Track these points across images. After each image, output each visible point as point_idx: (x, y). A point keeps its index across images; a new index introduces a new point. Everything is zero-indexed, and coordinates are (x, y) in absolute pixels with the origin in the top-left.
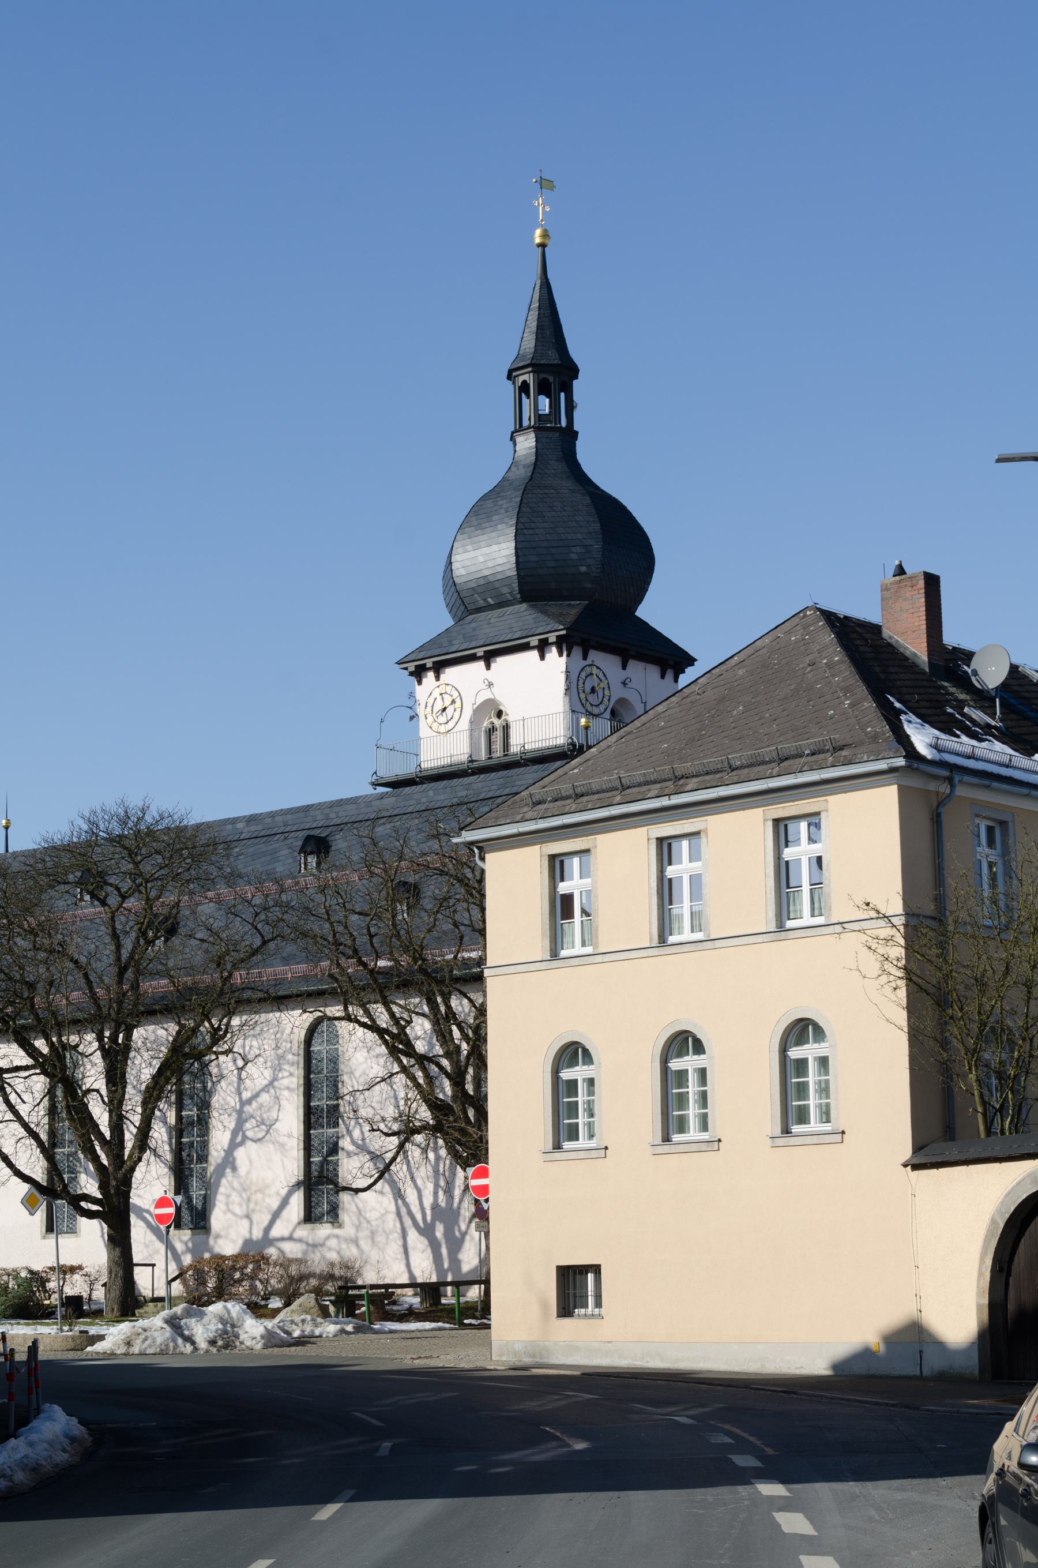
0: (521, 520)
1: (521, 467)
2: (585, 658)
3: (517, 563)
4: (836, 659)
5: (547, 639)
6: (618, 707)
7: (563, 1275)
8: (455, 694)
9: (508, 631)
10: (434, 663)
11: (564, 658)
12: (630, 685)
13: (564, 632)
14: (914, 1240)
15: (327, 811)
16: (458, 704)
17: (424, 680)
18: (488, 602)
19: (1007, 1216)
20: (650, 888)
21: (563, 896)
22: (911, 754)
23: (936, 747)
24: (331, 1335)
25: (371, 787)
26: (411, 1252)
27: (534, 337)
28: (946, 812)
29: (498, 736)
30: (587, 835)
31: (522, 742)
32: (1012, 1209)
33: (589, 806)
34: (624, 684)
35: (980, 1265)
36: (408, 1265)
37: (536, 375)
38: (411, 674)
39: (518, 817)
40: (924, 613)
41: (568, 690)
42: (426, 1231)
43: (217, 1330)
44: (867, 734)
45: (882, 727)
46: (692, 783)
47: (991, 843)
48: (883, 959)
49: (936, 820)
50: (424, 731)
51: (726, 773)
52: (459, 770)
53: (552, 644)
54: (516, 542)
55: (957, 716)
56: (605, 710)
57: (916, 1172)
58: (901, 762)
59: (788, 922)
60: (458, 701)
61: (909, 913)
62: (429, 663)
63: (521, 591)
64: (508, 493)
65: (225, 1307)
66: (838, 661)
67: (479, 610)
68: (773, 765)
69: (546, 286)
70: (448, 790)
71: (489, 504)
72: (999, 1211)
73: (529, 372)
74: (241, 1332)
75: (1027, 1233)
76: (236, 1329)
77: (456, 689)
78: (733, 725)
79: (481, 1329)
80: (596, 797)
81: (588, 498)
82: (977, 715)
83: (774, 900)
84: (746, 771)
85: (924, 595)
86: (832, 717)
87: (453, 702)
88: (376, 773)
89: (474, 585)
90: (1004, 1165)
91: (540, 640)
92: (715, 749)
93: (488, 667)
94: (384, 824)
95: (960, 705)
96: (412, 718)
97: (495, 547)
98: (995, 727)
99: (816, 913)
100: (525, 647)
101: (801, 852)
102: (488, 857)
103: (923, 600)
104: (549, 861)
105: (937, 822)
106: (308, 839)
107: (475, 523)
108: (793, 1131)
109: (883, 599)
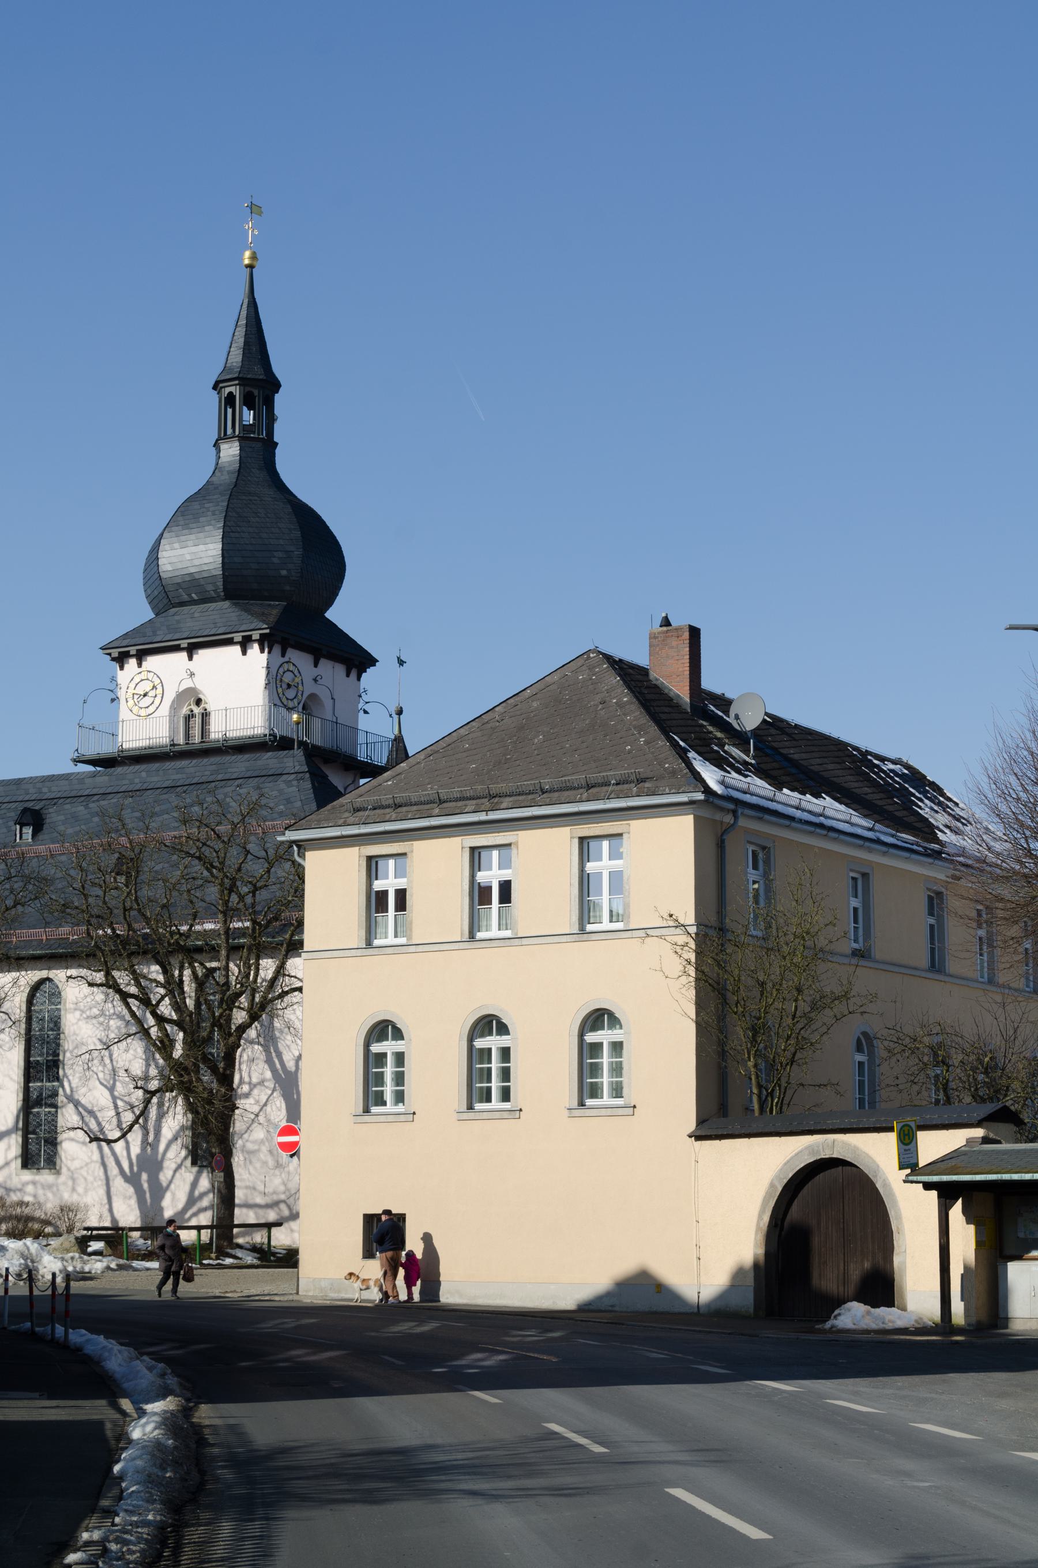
0: (227, 523)
1: (225, 473)
2: (283, 655)
3: (223, 563)
4: (625, 699)
5: (251, 636)
6: (308, 701)
7: (368, 1222)
8: (157, 681)
9: (212, 626)
10: (138, 650)
11: (266, 654)
12: (320, 682)
13: (268, 631)
14: (696, 1199)
15: (39, 785)
16: (159, 690)
17: (126, 666)
18: (192, 597)
19: (785, 1181)
20: (462, 891)
21: (377, 892)
22: (707, 790)
23: (722, 783)
24: (99, 1272)
25: (72, 763)
26: (114, 1199)
27: (241, 352)
28: (729, 839)
29: (196, 723)
30: (403, 841)
31: (224, 729)
32: (790, 1175)
33: (409, 816)
34: (315, 680)
35: (758, 1221)
36: (111, 1210)
37: (242, 388)
38: (113, 659)
39: (341, 822)
40: (688, 661)
41: (267, 685)
42: (132, 1179)
43: (20, 1264)
44: (665, 769)
45: (678, 764)
46: (506, 802)
47: (755, 867)
48: (686, 962)
49: (721, 845)
50: (124, 713)
51: (537, 795)
52: (161, 753)
53: (255, 641)
54: (223, 544)
55: (722, 753)
56: (299, 704)
57: (699, 1142)
58: (700, 796)
59: (588, 925)
60: (159, 687)
61: (699, 923)
62: (133, 650)
63: (225, 589)
64: (215, 497)
65: (25, 1244)
66: (627, 701)
67: (182, 604)
68: (581, 791)
69: (253, 304)
70: (161, 772)
71: (196, 506)
72: (777, 1177)
73: (236, 385)
74: (40, 1267)
75: (800, 1195)
76: (35, 1264)
77: (158, 677)
78: (536, 752)
79: (218, 1269)
80: (415, 808)
81: (289, 506)
82: (736, 752)
83: (577, 907)
84: (556, 794)
85: (688, 645)
86: (630, 752)
87: (154, 687)
88: (77, 750)
89: (179, 581)
90: (783, 1139)
91: (243, 637)
92: (522, 773)
93: (190, 658)
94: (98, 801)
95: (722, 746)
96: (113, 700)
97: (202, 547)
98: (751, 764)
99: (614, 919)
100: (229, 642)
101: (601, 865)
102: (308, 854)
103: (688, 649)
104: (367, 861)
105: (721, 846)
106: (25, 810)
107: (182, 523)
108: (587, 1104)
109: (650, 646)
